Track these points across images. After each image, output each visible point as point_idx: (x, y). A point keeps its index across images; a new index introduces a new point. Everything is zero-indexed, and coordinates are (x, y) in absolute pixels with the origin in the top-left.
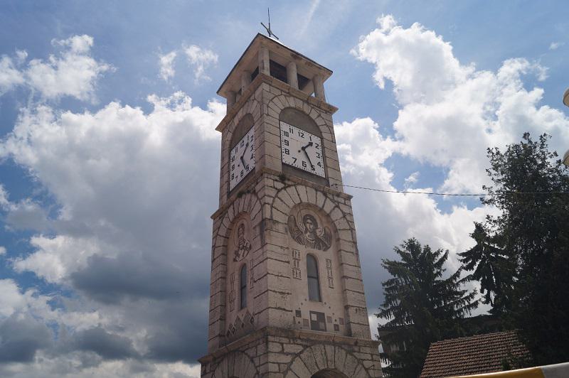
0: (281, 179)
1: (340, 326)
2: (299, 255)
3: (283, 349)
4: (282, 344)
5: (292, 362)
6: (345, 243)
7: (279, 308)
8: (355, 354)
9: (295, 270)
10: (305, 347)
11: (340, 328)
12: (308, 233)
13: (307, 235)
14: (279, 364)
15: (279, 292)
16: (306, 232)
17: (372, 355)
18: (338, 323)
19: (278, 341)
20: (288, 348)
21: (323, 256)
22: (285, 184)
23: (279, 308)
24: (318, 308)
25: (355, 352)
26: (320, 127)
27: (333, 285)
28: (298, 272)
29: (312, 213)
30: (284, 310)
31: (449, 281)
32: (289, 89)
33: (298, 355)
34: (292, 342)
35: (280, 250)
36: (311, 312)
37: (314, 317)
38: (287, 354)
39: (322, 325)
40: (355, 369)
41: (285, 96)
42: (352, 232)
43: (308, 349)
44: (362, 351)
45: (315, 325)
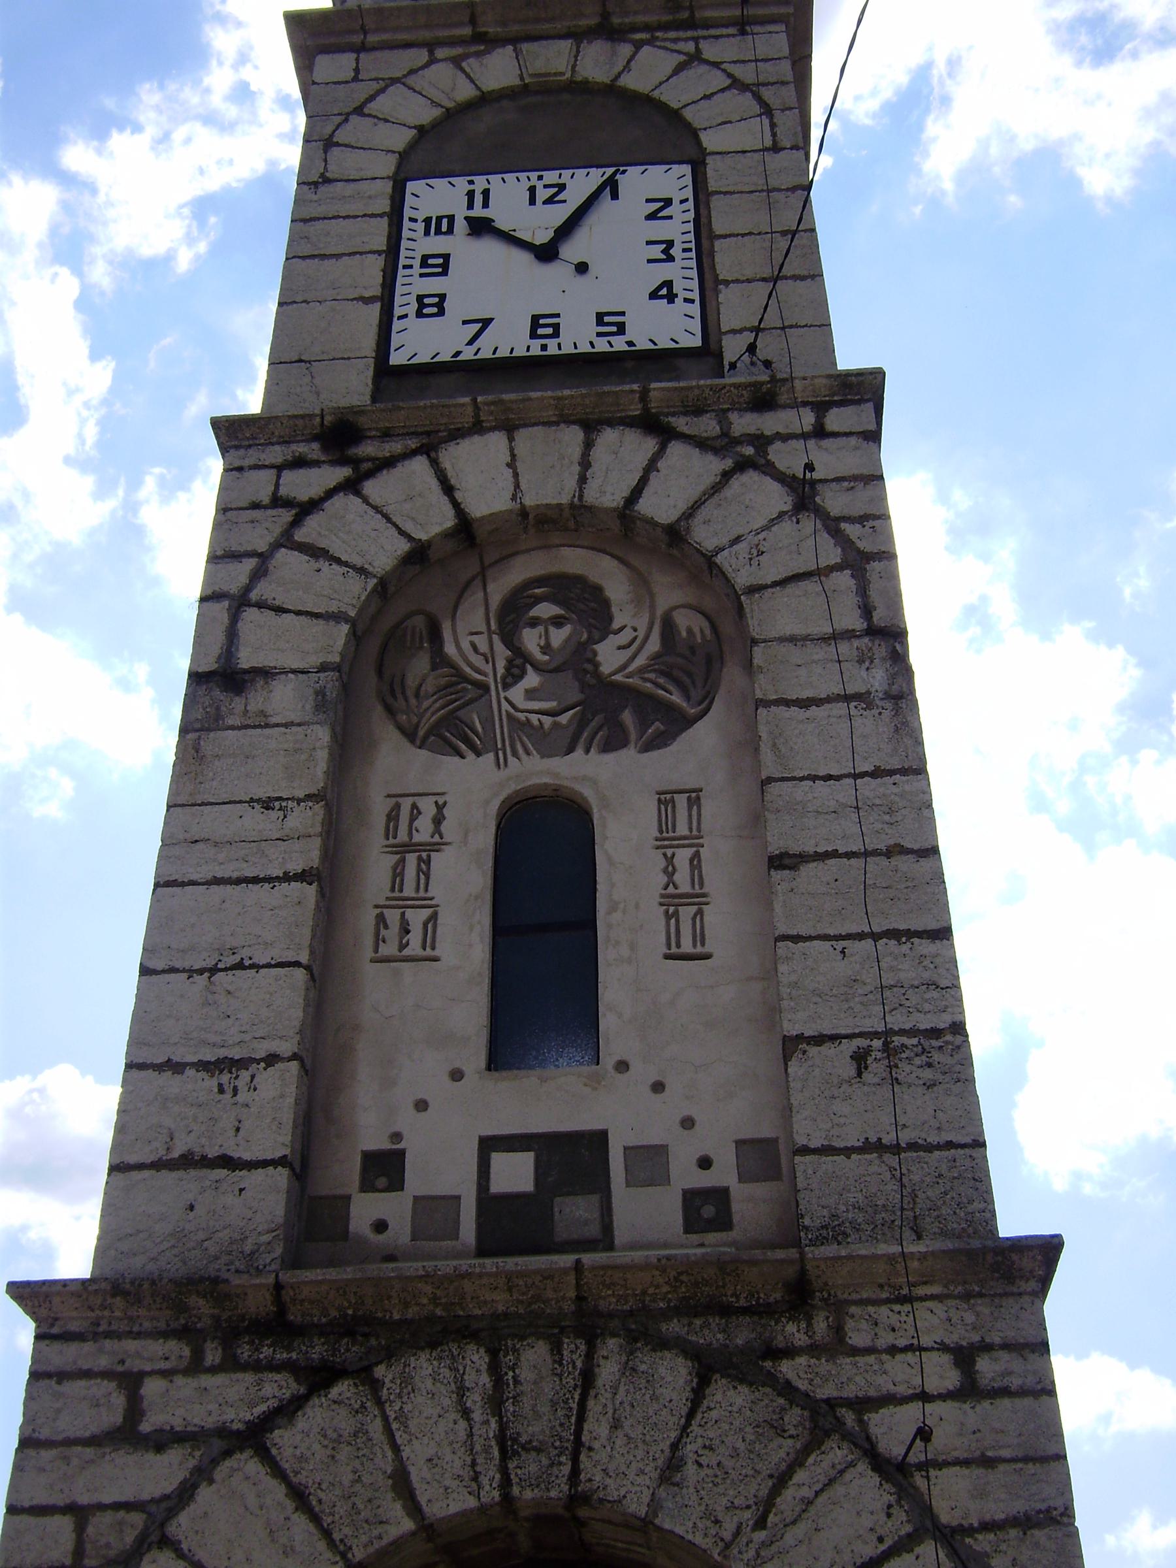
0: (325, 448)
1: (739, 1191)
2: (438, 820)
3: (135, 1410)
4: (131, 1382)
5: (185, 1494)
6: (794, 654)
7: (188, 1161)
8: (787, 1369)
9: (393, 916)
10: (319, 1378)
11: (737, 1207)
12: (532, 679)
13: (517, 694)
14: (79, 1513)
15: (204, 1066)
16: (513, 676)
17: (964, 1357)
18: (724, 1174)
19: (103, 1362)
20: (177, 1402)
21: (620, 788)
22: (354, 462)
23: (188, 1161)
24: (551, 1100)
25: (790, 1352)
26: (688, 114)
27: (700, 937)
28: (417, 918)
29: (573, 560)
30: (227, 1162)
31: (135, 484)
32: (473, 21)
33: (253, 1437)
34: (213, 1355)
35: (256, 822)
36: (489, 1145)
37: (515, 1173)
38: (161, 1441)
39: (575, 1212)
40: (781, 1480)
41: (457, 62)
42: (861, 577)
43: (342, 1389)
44: (858, 1337)
45: (510, 1225)
